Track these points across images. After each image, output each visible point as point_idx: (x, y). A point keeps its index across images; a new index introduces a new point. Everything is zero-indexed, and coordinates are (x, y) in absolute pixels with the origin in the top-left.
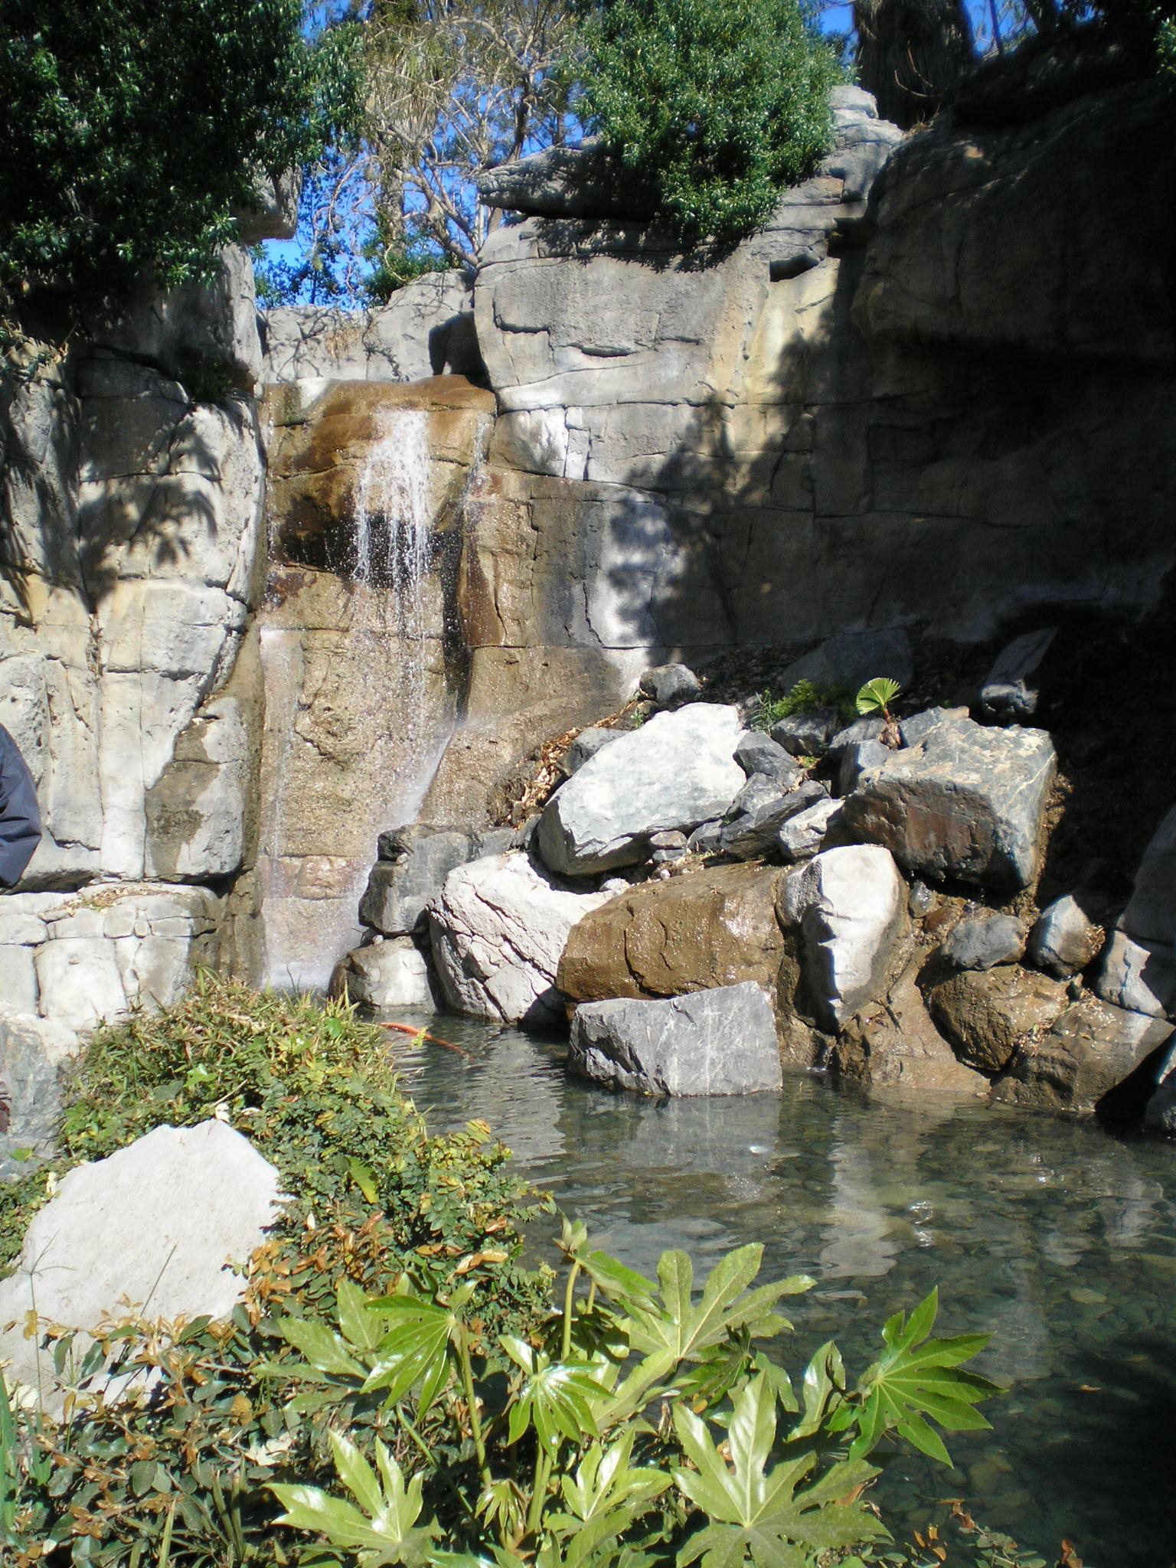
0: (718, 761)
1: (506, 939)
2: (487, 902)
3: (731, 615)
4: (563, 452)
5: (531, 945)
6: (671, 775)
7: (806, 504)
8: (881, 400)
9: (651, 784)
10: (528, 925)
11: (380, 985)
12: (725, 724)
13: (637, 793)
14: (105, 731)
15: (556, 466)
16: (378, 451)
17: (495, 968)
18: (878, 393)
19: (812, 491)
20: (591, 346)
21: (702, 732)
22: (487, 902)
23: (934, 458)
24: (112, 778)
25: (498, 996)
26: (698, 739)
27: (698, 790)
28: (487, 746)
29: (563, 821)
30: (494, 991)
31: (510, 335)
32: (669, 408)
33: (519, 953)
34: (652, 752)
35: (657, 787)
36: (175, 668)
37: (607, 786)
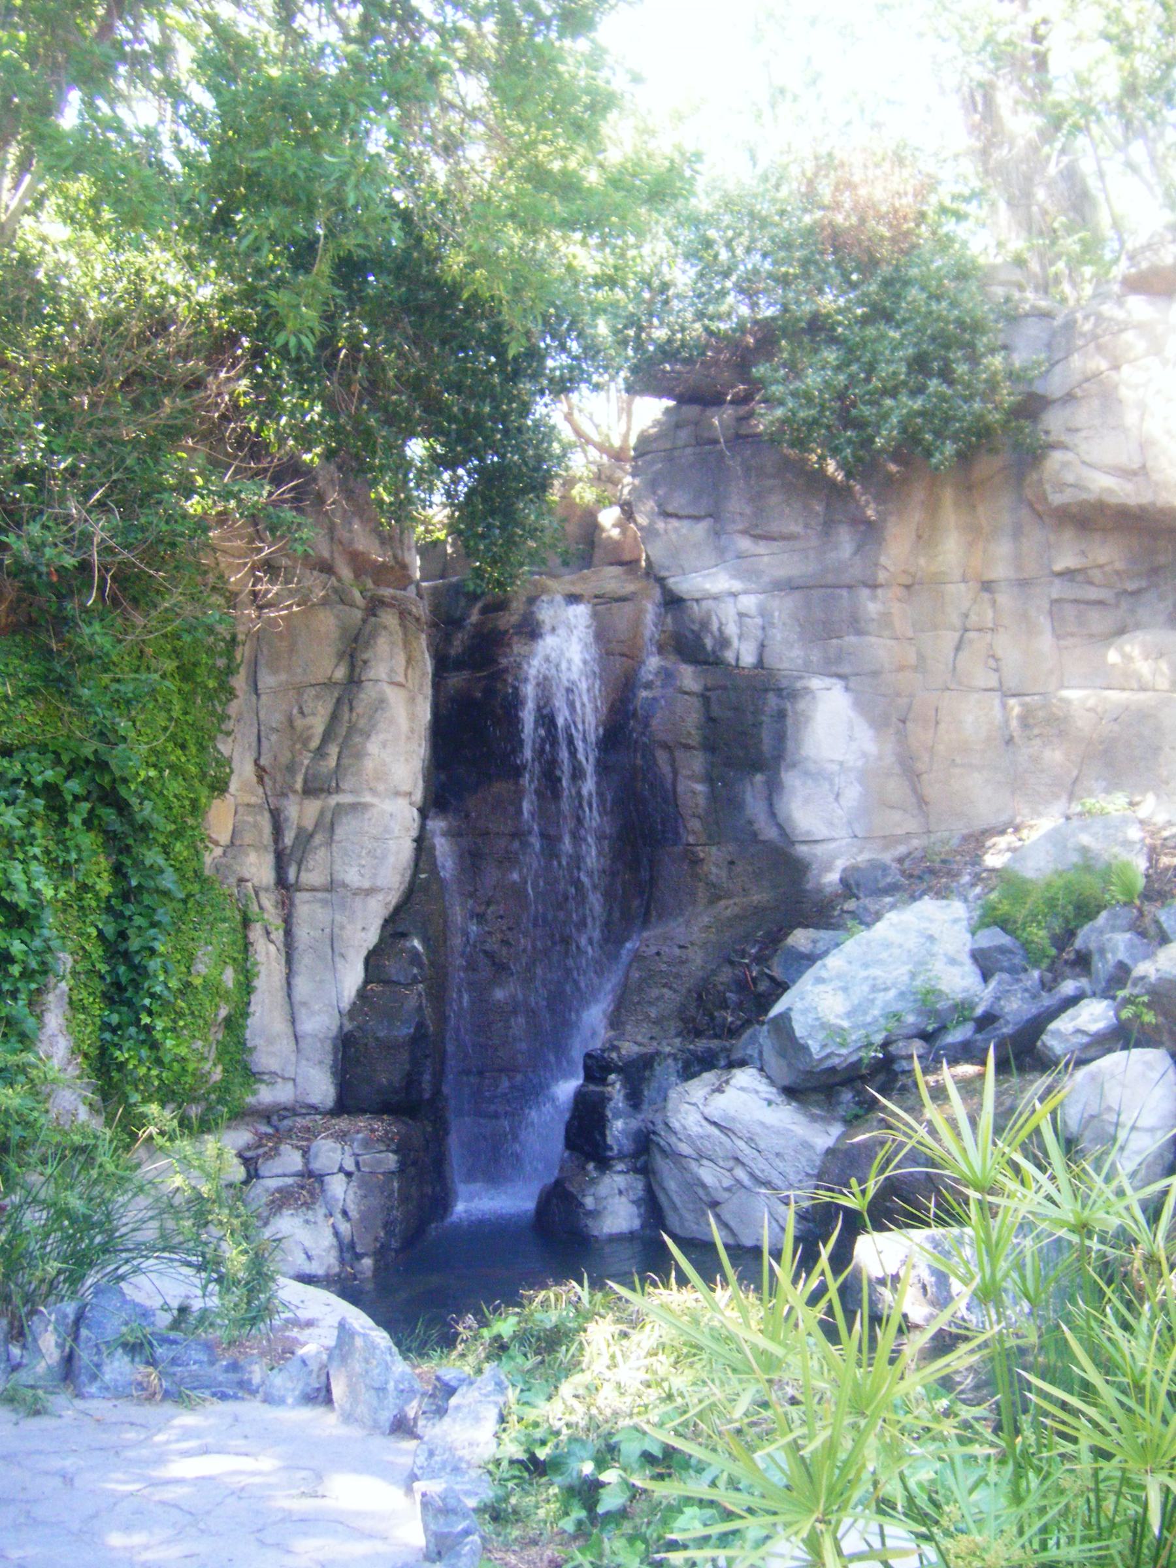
0: (953, 961)
1: (737, 1159)
2: (715, 1124)
3: (922, 802)
4: (735, 642)
5: (767, 1167)
6: (906, 978)
7: (993, 682)
8: (1060, 574)
9: (886, 989)
10: (762, 1146)
11: (595, 1214)
12: (956, 921)
13: (872, 1001)
14: (296, 956)
15: (729, 656)
16: (549, 643)
17: (726, 1195)
18: (1058, 567)
19: (996, 670)
20: (759, 532)
21: (934, 930)
22: (715, 1124)
23: (1121, 631)
24: (304, 1004)
25: (732, 1224)
26: (931, 938)
27: (933, 992)
28: (677, 951)
29: (798, 1034)
30: (727, 1217)
31: (675, 523)
32: (844, 592)
33: (752, 1175)
34: (884, 955)
35: (892, 993)
36: (366, 885)
37: (841, 996)
